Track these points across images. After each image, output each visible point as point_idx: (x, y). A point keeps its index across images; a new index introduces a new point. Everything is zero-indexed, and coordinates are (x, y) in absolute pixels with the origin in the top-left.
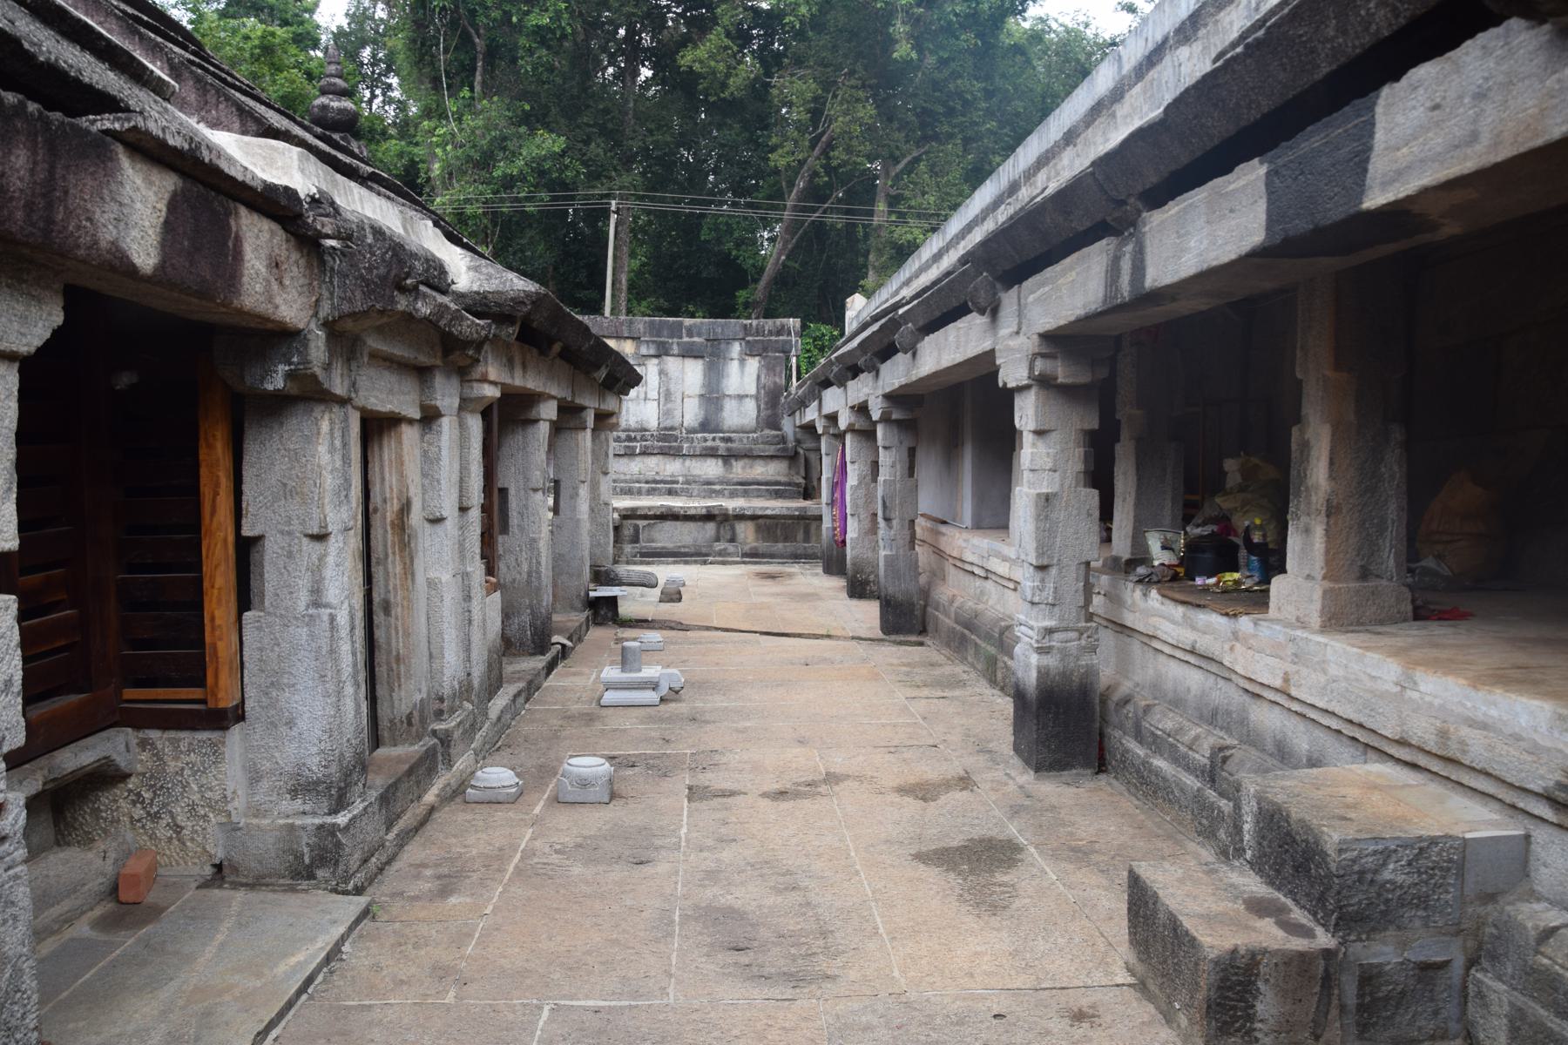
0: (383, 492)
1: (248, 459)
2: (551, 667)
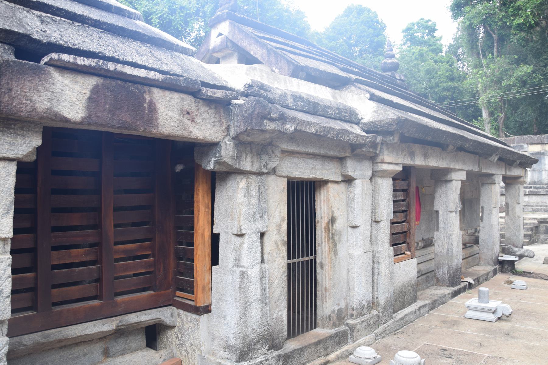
0: (321, 214)
2: (455, 294)
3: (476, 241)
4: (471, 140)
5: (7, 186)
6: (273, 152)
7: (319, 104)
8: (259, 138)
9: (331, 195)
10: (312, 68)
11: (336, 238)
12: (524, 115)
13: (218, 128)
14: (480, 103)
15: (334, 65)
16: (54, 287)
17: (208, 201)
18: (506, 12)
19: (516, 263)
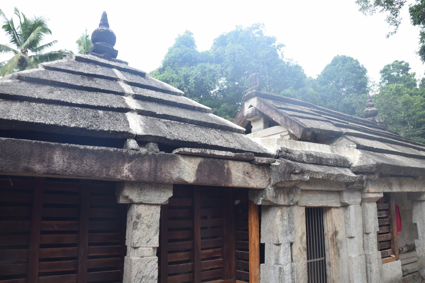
0: (327, 229)
1: (262, 222)
5: (156, 219)
6: (296, 192)
7: (323, 158)
8: (288, 185)
9: (334, 216)
10: (315, 128)
15: (329, 122)
16: (170, 275)
17: (257, 223)
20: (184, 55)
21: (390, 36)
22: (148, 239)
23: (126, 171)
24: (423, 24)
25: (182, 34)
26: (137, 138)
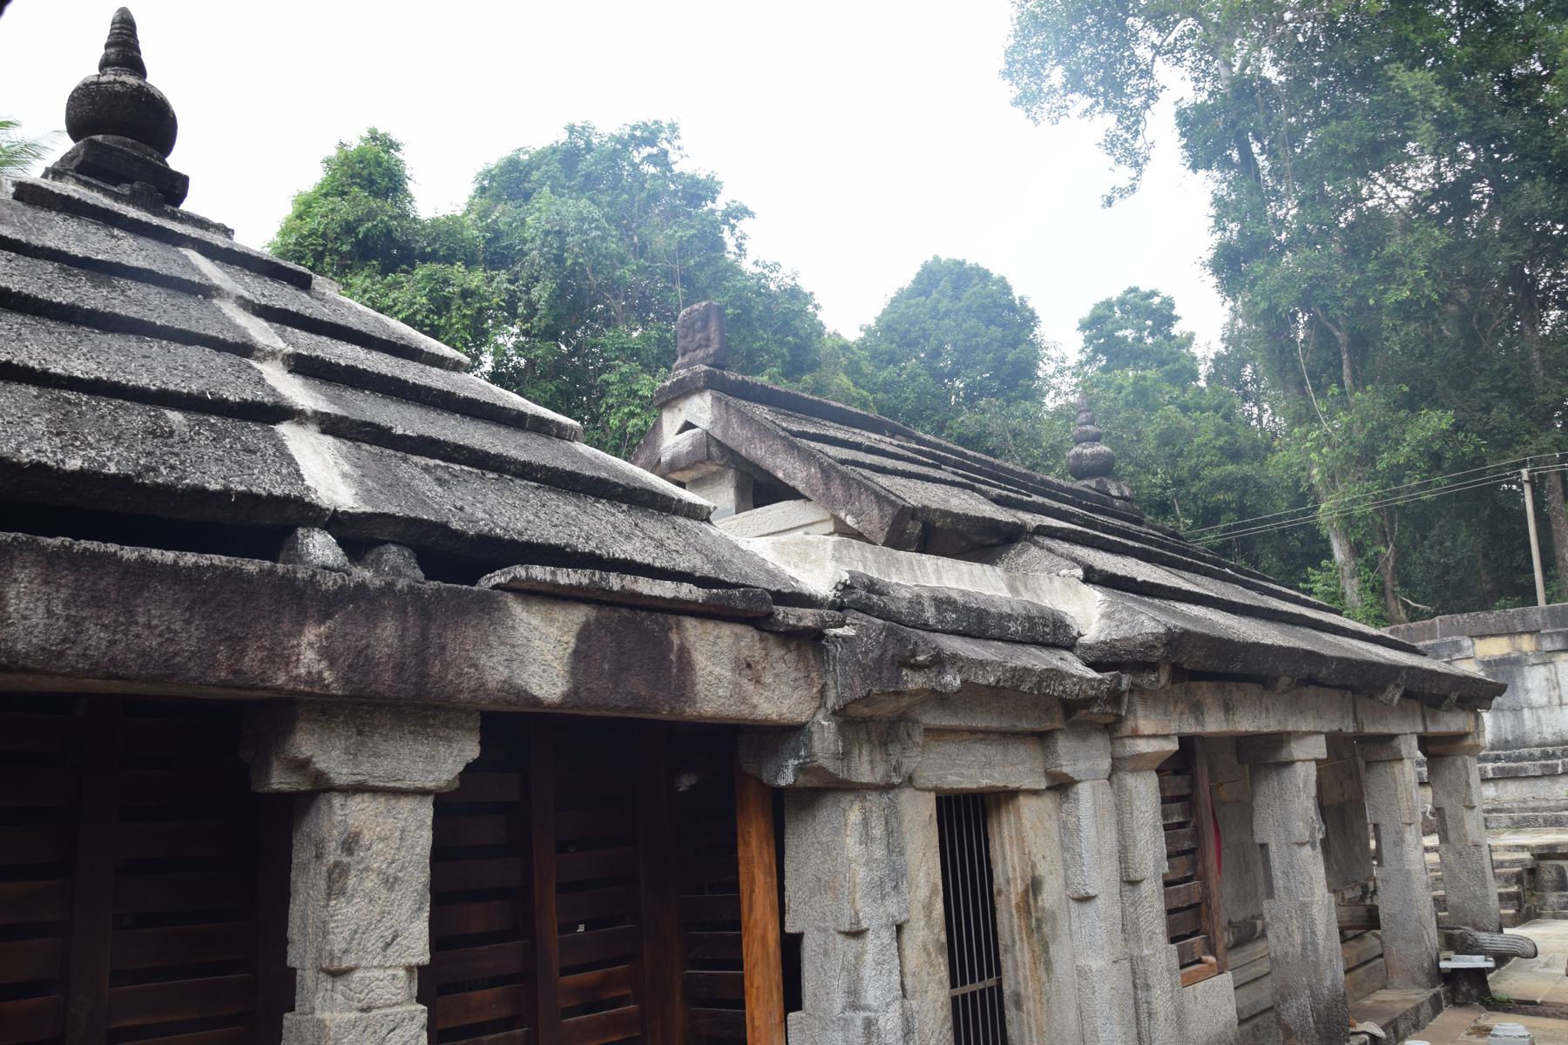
0: (1005, 872)
3: (1372, 920)
4: (1332, 658)
5: (418, 850)
7: (988, 613)
8: (888, 708)
9: (1027, 824)
11: (1046, 929)
12: (1448, 544)
13: (804, 693)
14: (1323, 519)
15: (973, 489)
17: (769, 857)
18: (1363, 271)
19: (1489, 977)
20: (362, 230)
21: (1117, 202)
22: (388, 934)
23: (309, 655)
24: (1218, 168)
25: (354, 142)
26: (338, 524)
